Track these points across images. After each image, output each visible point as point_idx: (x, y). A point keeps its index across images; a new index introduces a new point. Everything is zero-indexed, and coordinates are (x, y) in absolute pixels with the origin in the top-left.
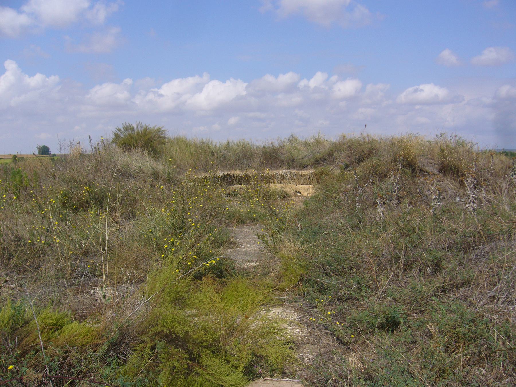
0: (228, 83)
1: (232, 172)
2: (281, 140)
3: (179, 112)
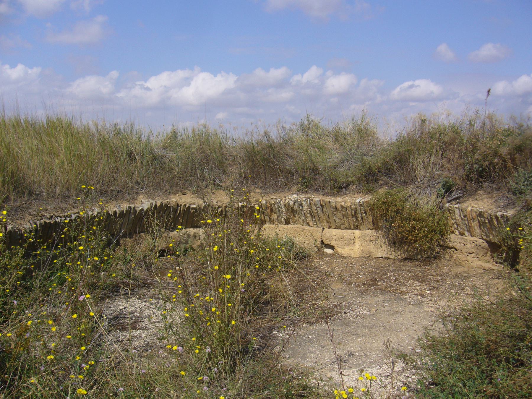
0: (219, 78)
1: (176, 199)
2: (284, 128)
3: (164, 106)
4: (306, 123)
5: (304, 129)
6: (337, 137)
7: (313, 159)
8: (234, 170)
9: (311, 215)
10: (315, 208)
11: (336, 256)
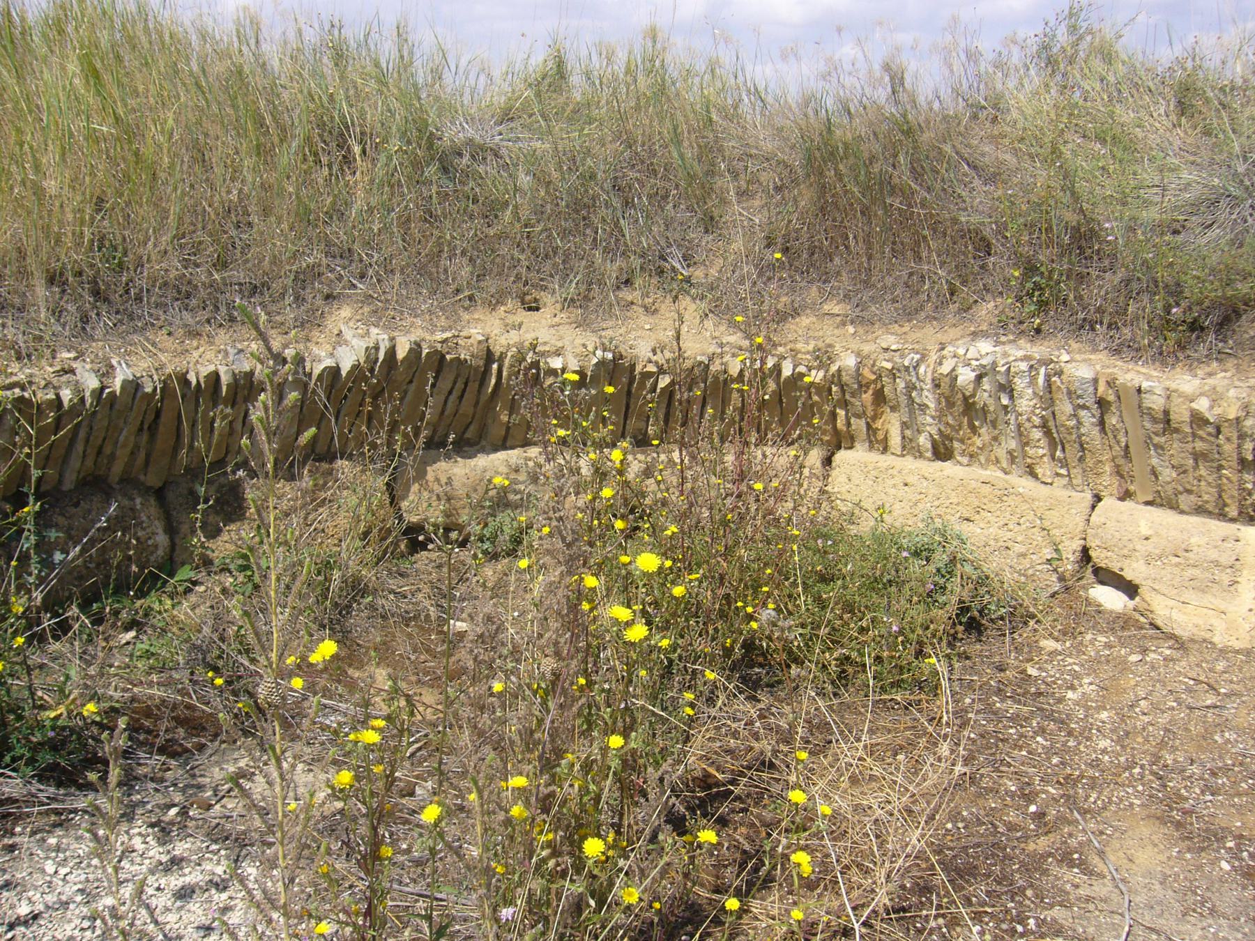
1: (492, 330)
2: (972, 56)
4: (1062, 36)
5: (1051, 62)
6: (1187, 97)
7: (1081, 186)
8: (746, 218)
9: (1048, 433)
10: (1068, 409)
11: (1140, 629)
